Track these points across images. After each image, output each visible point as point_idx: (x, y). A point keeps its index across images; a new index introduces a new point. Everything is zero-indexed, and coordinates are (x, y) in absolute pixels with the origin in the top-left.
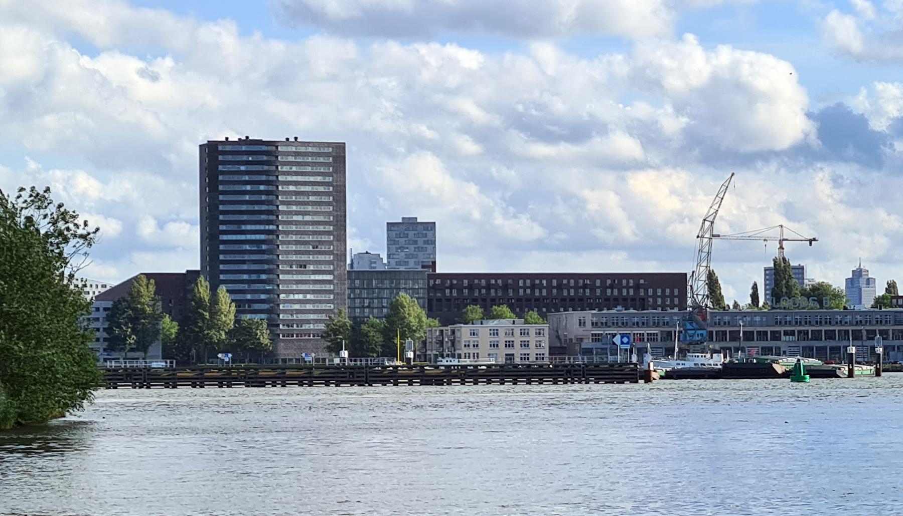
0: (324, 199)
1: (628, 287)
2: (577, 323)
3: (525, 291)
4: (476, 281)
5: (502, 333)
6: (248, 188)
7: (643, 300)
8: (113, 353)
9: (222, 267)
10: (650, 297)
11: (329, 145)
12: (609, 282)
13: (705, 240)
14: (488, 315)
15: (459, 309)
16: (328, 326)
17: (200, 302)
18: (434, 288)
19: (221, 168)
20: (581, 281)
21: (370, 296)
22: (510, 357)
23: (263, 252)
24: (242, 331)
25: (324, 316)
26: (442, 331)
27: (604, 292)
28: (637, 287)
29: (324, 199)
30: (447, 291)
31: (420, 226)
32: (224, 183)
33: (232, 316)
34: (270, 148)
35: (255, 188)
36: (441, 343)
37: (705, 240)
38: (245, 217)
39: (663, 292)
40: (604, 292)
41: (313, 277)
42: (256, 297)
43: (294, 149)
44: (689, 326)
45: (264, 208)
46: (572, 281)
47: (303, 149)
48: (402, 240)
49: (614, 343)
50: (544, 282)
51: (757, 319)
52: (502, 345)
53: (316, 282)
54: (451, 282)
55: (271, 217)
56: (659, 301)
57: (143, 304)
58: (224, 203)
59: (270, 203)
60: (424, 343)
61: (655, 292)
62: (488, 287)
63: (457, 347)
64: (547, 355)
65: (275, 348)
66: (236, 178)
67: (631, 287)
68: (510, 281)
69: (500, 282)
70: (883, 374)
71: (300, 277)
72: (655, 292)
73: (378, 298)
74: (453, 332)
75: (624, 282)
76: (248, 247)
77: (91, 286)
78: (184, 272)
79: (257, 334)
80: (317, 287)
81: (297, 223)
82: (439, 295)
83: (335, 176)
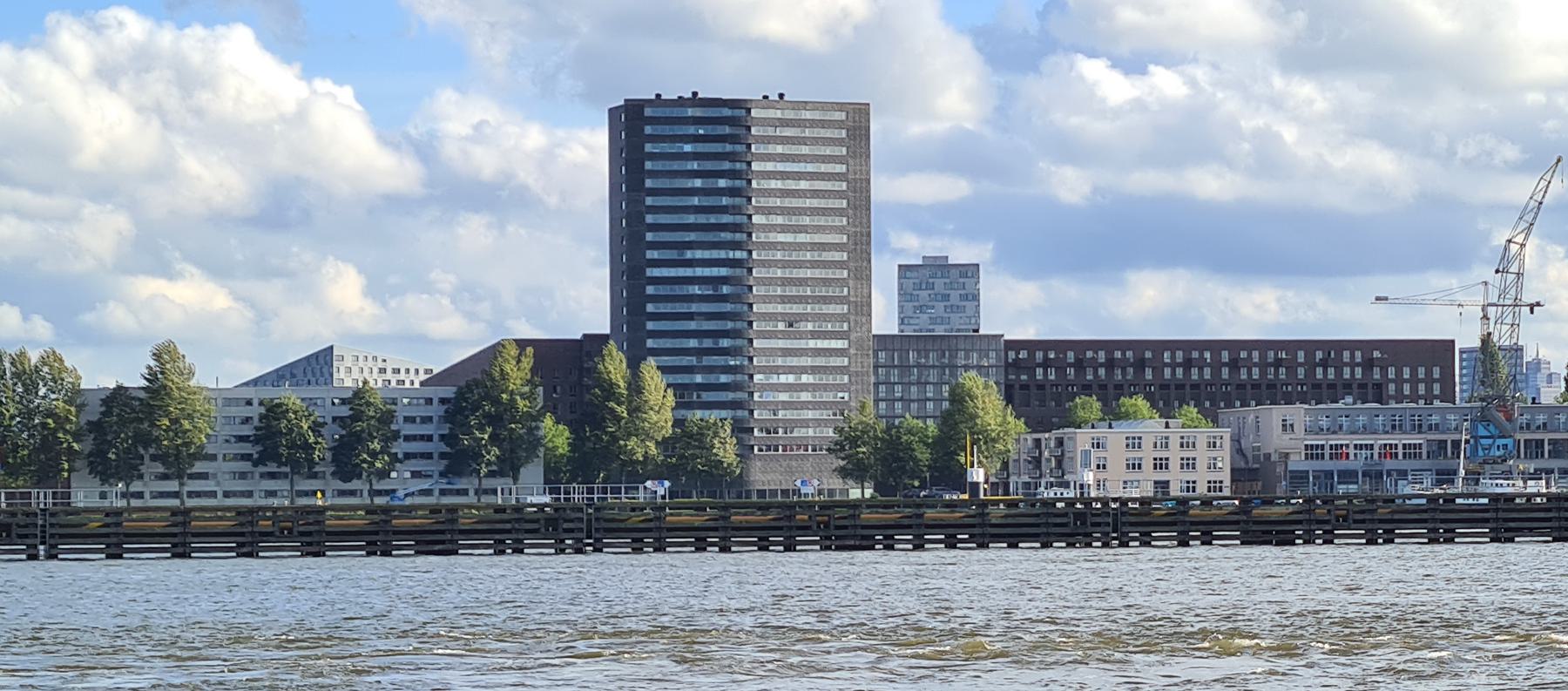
1: (1353, 365)
2: (1286, 430)
4: (1089, 354)
5: (1147, 443)
6: (698, 183)
8: (456, 480)
10: (1391, 381)
11: (840, 106)
12: (1319, 355)
14: (1113, 414)
16: (839, 431)
17: (609, 390)
18: (1016, 365)
19: (648, 148)
20: (1271, 354)
21: (906, 380)
22: (1163, 485)
23: (723, 298)
27: (1311, 372)
28: (1368, 364)
30: (1039, 371)
32: (654, 174)
35: (710, 183)
36: (1037, 462)
38: (692, 236)
39: (1414, 372)
40: (1311, 372)
41: (812, 344)
42: (712, 379)
43: (779, 114)
44: (1482, 432)
46: (1256, 354)
47: (790, 114)
48: (924, 294)
50: (1207, 355)
52: (1148, 465)
53: (818, 352)
54: (1045, 356)
55: (738, 236)
56: (1422, 388)
58: (654, 210)
59: (736, 210)
61: (1399, 373)
62: (1110, 364)
64: (1227, 483)
66: (676, 166)
67: (1358, 365)
68: (1148, 355)
69: (1129, 354)
72: (1399, 373)
73: (918, 383)
75: (1346, 354)
77: (408, 371)
78: (579, 337)
79: (713, 446)
80: (820, 361)
81: (784, 246)
82: (1024, 377)
83: (851, 162)
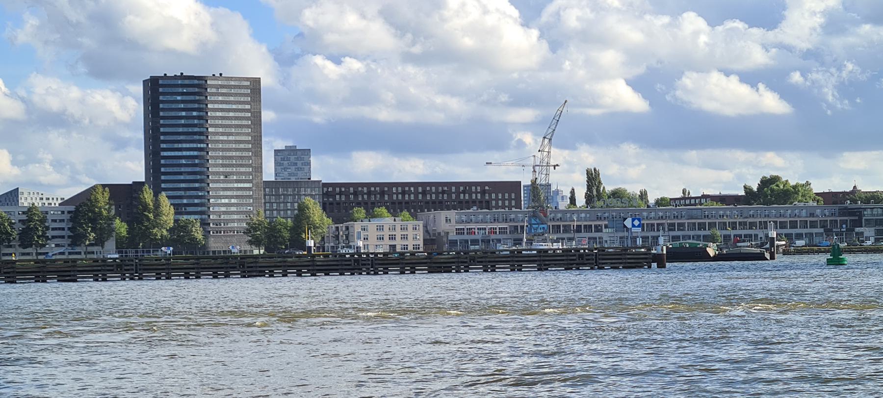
0: (245, 122)
1: (476, 193)
2: (447, 222)
3: (375, 197)
4: (360, 189)
5: (386, 228)
6: (184, 114)
7: (488, 202)
9: (163, 177)
11: (247, 79)
12: (462, 188)
13: (545, 154)
14: (370, 215)
15: (347, 211)
16: (248, 224)
17: (146, 207)
19: (161, 98)
23: (195, 165)
24: (179, 228)
25: (242, 217)
26: (337, 228)
27: (458, 196)
28: (483, 192)
29: (245, 122)
30: (338, 197)
31: (299, 153)
32: (163, 110)
33: (172, 217)
34: (201, 82)
35: (189, 114)
36: (337, 237)
37: (545, 154)
38: (182, 138)
39: (503, 196)
40: (458, 196)
41: (236, 185)
42: (191, 201)
44: (533, 222)
45: (196, 130)
46: (433, 188)
49: (625, 226)
50: (412, 189)
51: (583, 215)
52: (386, 238)
53: (238, 189)
55: (202, 138)
56: (507, 203)
57: (100, 208)
59: (201, 126)
60: (323, 238)
62: (369, 193)
63: (350, 238)
64: (422, 245)
65: (207, 242)
66: (173, 106)
68: (386, 189)
70: (848, 258)
71: (225, 185)
72: (497, 196)
74: (347, 228)
75: (473, 188)
76: (184, 162)
78: (131, 183)
80: (239, 193)
81: (222, 142)
